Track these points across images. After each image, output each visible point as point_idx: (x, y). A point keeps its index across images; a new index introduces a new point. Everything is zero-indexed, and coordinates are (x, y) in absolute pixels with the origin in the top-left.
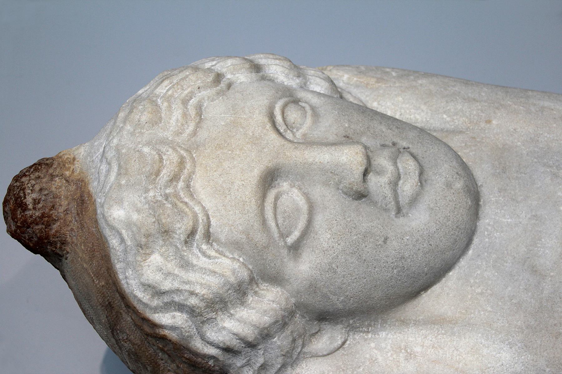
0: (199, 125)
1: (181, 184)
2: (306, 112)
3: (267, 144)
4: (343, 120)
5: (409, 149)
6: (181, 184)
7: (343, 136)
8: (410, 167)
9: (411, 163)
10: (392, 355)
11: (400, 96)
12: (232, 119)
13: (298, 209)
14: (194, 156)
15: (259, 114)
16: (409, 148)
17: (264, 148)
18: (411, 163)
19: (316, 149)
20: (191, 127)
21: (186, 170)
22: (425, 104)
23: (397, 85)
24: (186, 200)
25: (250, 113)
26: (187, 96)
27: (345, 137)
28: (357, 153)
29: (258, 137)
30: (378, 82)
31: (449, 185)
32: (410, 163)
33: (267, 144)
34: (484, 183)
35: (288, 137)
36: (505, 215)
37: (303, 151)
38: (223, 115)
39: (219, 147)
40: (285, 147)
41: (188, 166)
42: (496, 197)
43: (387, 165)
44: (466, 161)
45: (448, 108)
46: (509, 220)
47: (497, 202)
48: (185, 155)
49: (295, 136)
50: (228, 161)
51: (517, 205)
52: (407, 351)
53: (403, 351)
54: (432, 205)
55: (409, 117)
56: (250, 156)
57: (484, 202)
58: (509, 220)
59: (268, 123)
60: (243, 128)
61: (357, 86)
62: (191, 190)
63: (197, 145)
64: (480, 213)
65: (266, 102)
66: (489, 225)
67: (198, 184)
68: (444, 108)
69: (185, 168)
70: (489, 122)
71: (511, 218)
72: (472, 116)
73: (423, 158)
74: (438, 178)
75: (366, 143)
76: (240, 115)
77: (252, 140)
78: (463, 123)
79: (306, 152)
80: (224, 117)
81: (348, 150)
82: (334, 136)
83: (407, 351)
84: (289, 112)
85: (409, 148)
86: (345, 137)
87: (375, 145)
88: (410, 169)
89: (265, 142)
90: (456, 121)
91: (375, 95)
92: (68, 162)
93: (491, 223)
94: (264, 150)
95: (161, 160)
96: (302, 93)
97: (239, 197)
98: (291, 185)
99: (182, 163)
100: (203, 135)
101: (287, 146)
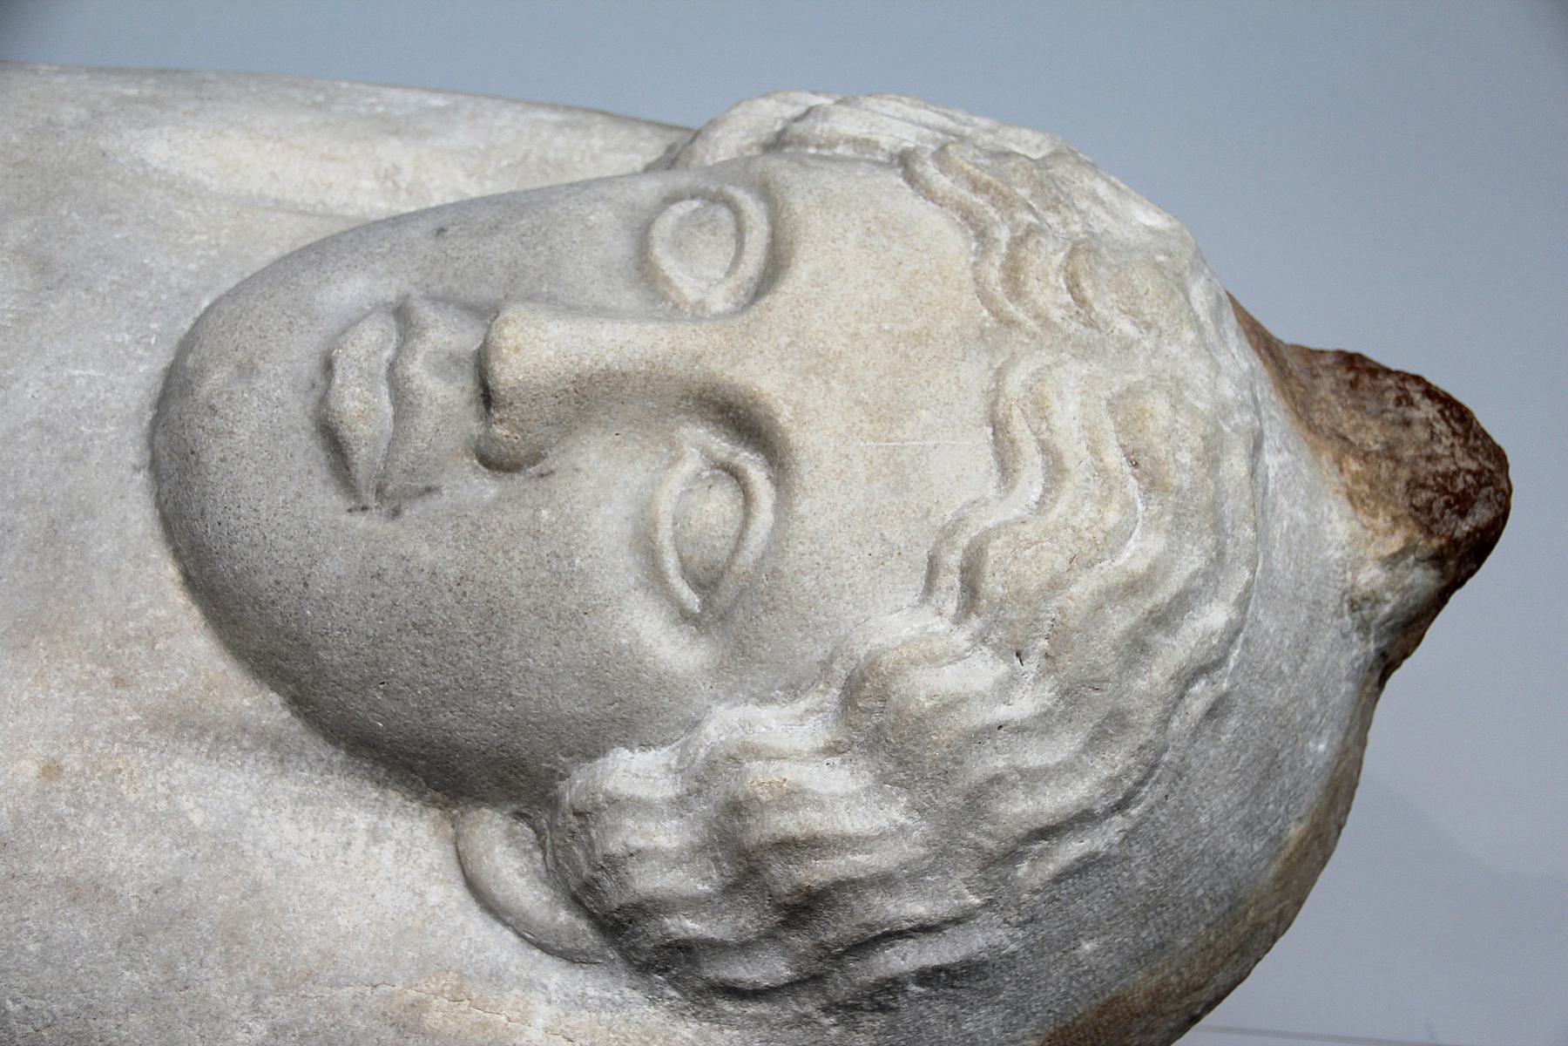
0: (995, 396)
1: (1003, 234)
2: (675, 538)
3: (781, 359)
4: (555, 531)
5: (349, 507)
6: (1003, 234)
7: (557, 474)
8: (358, 390)
9: (351, 405)
10: (432, 180)
11: (343, 930)
12: (899, 432)
13: (677, 245)
14: (985, 313)
15: (820, 452)
16: (350, 511)
17: (791, 344)
18: (351, 405)
19: (637, 356)
20: (1015, 382)
21: (997, 263)
22: (256, 888)
23: (347, 993)
24: (979, 200)
25: (847, 456)
26: (1054, 501)
27: (552, 472)
28: (517, 350)
29: (812, 377)
30: (418, 1006)
31: (247, 371)
32: (356, 403)
33: (781, 359)
34: (128, 478)
35: (724, 444)
36: (88, 383)
37: (674, 349)
38: (930, 443)
39: (920, 338)
40: (729, 356)
41: (994, 274)
42: (100, 436)
43: (425, 376)
44: (166, 567)
45: (177, 854)
46: (77, 373)
47: (102, 420)
48: (1011, 307)
49: (702, 452)
50: (886, 302)
51: (42, 416)
52: (395, 183)
53: (403, 185)
54: (303, 321)
55: (319, 835)
56: (826, 316)
57: (141, 419)
58: (77, 373)
59: (787, 425)
60: (858, 402)
61: (496, 977)
62: (971, 232)
63: (985, 341)
64: (159, 387)
65: (803, 507)
66: (141, 360)
67: (955, 244)
68: (194, 858)
69: (1003, 267)
70: (51, 770)
71: (72, 378)
72: (101, 805)
73: (310, 472)
74: (274, 391)
75: (484, 484)
76: (877, 448)
77: (829, 366)
78: (140, 776)
79: (664, 346)
80: (924, 438)
81: (544, 357)
82: (584, 466)
83: (395, 183)
84: (729, 515)
85: (350, 511)
86: (552, 472)
87: (457, 486)
88: (360, 385)
89: (788, 363)
90: (161, 789)
91: (433, 935)
92: (1368, 501)
93: (131, 364)
94: (788, 340)
95: (1074, 287)
96: (691, 661)
97: (841, 215)
98: (703, 309)
99: (1015, 288)
100: (974, 373)
101: (722, 362)
